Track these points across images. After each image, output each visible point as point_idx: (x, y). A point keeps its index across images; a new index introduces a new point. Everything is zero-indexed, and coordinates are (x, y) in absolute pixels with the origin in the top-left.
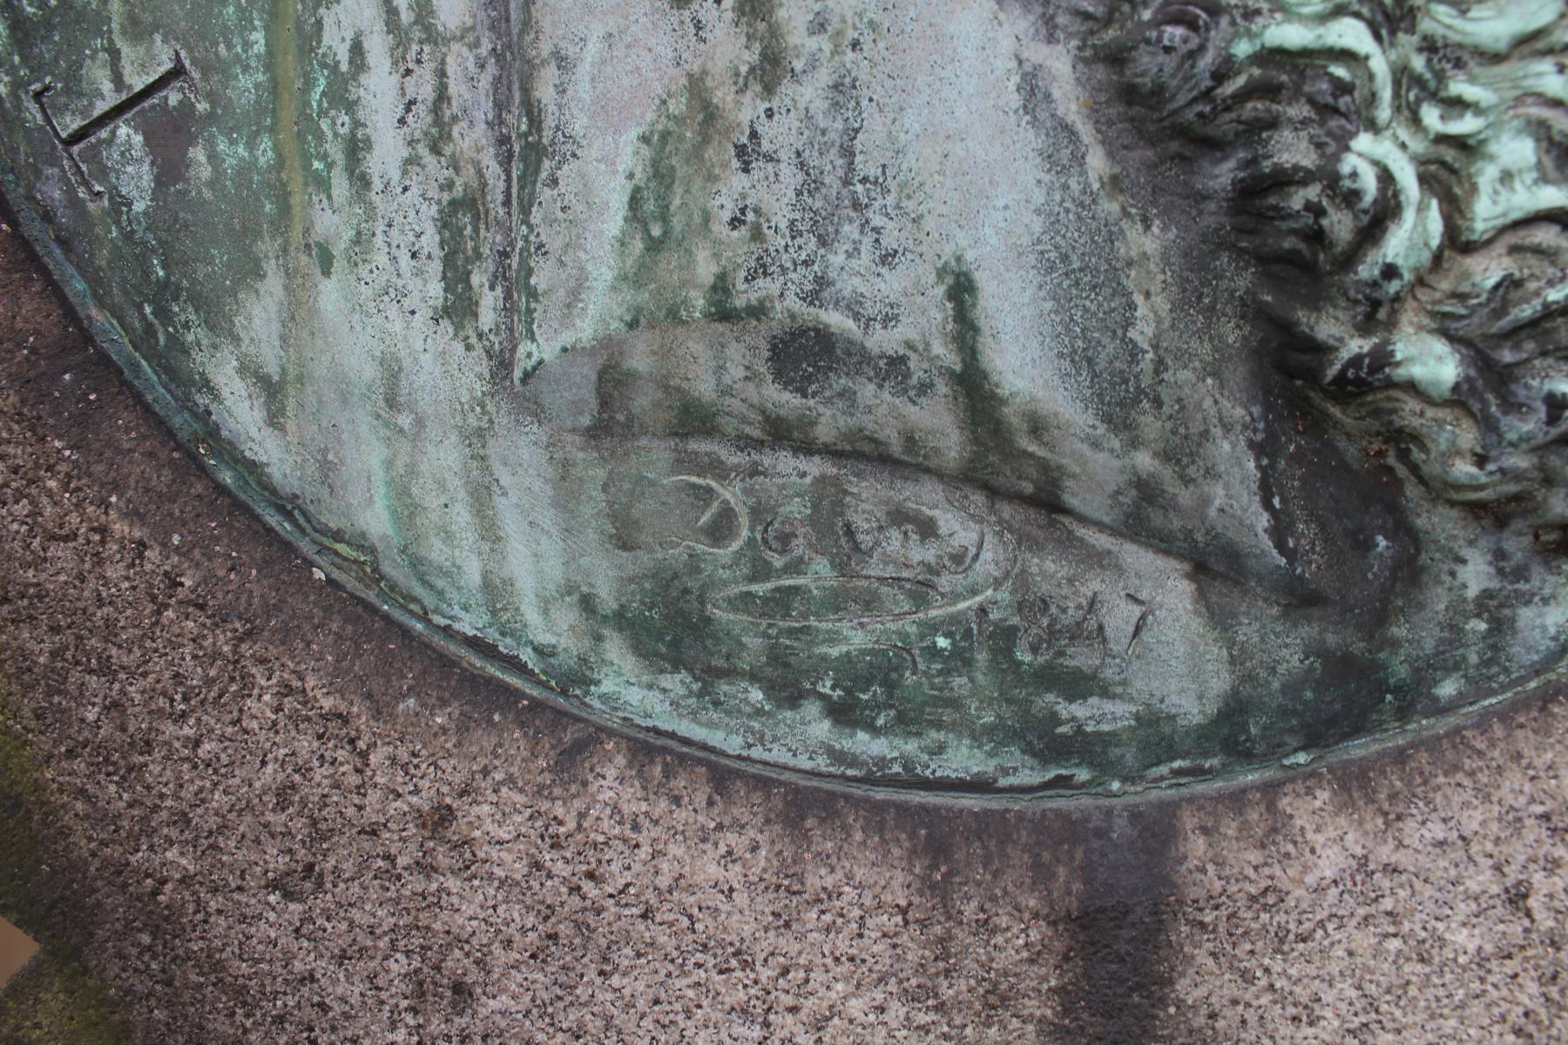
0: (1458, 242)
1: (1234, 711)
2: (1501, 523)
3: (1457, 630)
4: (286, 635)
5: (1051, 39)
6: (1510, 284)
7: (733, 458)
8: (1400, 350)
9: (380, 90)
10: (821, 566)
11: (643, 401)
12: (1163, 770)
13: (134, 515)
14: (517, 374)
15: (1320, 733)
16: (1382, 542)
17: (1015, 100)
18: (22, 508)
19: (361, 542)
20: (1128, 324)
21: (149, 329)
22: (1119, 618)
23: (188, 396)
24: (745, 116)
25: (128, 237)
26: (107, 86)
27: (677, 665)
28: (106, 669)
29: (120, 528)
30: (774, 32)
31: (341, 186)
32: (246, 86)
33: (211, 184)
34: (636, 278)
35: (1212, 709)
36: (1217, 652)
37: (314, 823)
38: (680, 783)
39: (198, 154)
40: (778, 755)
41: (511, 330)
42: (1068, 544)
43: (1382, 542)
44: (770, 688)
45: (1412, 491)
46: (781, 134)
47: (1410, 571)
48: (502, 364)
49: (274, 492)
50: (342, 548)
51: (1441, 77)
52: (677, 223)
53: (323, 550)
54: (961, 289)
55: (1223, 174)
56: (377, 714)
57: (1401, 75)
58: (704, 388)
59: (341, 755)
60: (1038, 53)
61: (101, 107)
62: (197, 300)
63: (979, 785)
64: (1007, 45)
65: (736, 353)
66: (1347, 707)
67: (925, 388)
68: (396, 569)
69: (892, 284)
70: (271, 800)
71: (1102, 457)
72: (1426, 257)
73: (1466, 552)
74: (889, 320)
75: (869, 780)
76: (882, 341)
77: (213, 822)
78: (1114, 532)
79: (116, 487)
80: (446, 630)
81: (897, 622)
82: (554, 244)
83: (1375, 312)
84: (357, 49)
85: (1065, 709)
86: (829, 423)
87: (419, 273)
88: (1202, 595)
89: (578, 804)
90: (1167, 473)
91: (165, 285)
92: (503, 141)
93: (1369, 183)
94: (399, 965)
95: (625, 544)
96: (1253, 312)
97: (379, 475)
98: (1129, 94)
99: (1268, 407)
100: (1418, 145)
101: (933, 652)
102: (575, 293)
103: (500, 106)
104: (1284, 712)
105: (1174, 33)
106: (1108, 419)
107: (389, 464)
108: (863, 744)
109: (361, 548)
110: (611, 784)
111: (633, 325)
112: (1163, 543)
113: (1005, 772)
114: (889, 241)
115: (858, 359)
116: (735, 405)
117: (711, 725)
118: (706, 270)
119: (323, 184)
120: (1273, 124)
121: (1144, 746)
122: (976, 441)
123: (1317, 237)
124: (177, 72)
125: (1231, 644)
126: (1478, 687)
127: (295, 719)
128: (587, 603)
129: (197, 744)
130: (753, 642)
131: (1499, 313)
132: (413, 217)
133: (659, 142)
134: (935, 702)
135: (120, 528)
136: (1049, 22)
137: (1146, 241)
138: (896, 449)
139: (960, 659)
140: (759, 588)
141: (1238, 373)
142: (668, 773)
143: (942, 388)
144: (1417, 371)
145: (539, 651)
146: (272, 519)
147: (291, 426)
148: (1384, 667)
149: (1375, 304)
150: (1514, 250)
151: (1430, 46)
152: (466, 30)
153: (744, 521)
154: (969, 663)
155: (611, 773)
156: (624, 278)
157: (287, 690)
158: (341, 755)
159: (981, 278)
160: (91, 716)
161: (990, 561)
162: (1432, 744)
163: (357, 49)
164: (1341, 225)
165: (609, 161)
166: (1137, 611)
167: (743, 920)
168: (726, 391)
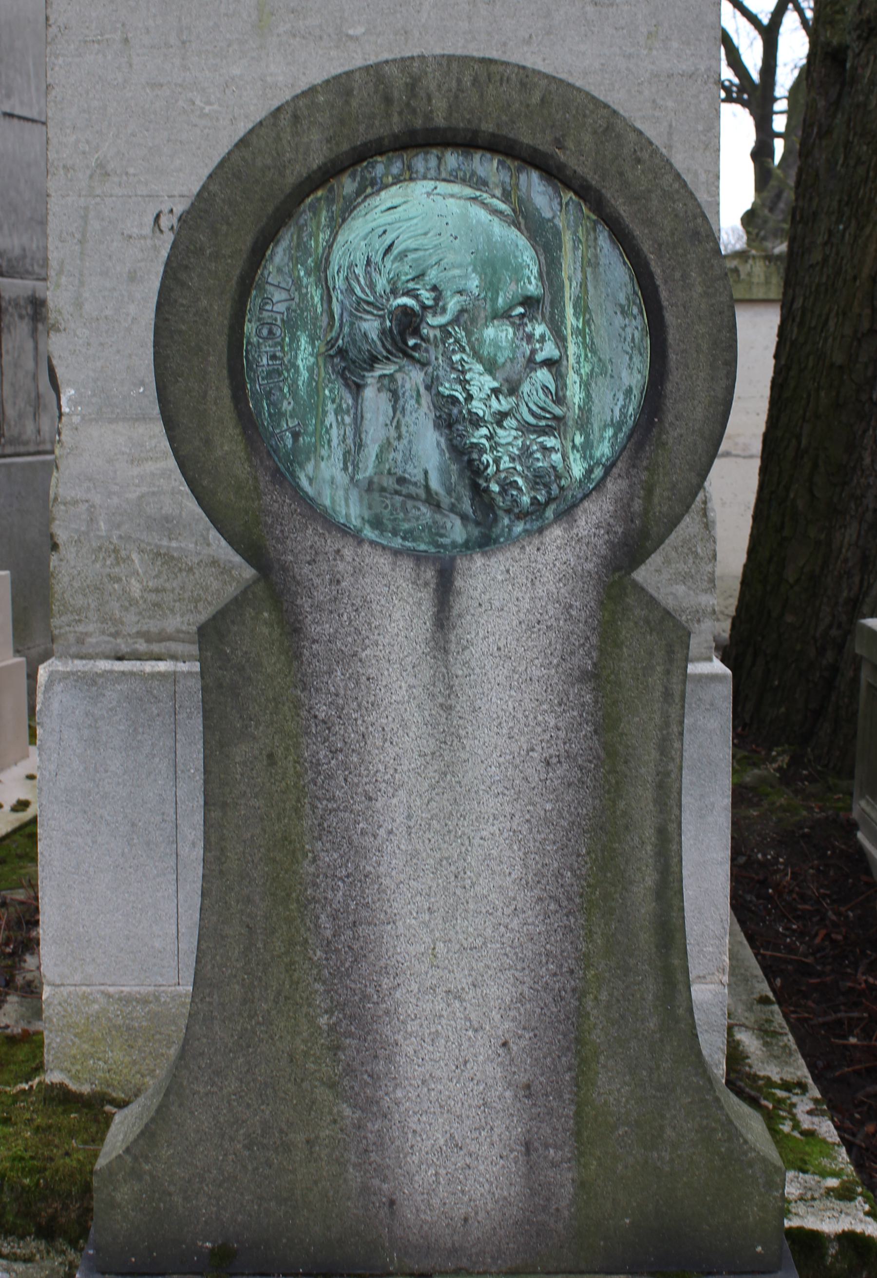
1: (467, 542)
9: (334, 432)
15: (481, 546)
19: (325, 506)
22: (449, 525)
28: (281, 524)
31: (326, 447)
32: (311, 429)
34: (376, 467)
39: (301, 439)
42: (441, 513)
46: (400, 447)
47: (496, 520)
48: (352, 479)
54: (426, 473)
55: (466, 458)
57: (491, 447)
58: (385, 485)
63: (426, 551)
66: (485, 542)
68: (330, 511)
69: (416, 471)
76: (413, 479)
81: (414, 524)
83: (487, 480)
86: (404, 491)
94: (328, 577)
96: (470, 478)
108: (407, 544)
110: (366, 547)
112: (456, 513)
115: (410, 482)
118: (387, 467)
126: (507, 540)
128: (363, 518)
132: (338, 453)
139: (423, 530)
141: (468, 488)
161: (428, 515)
164: (482, 467)
167: (387, 569)
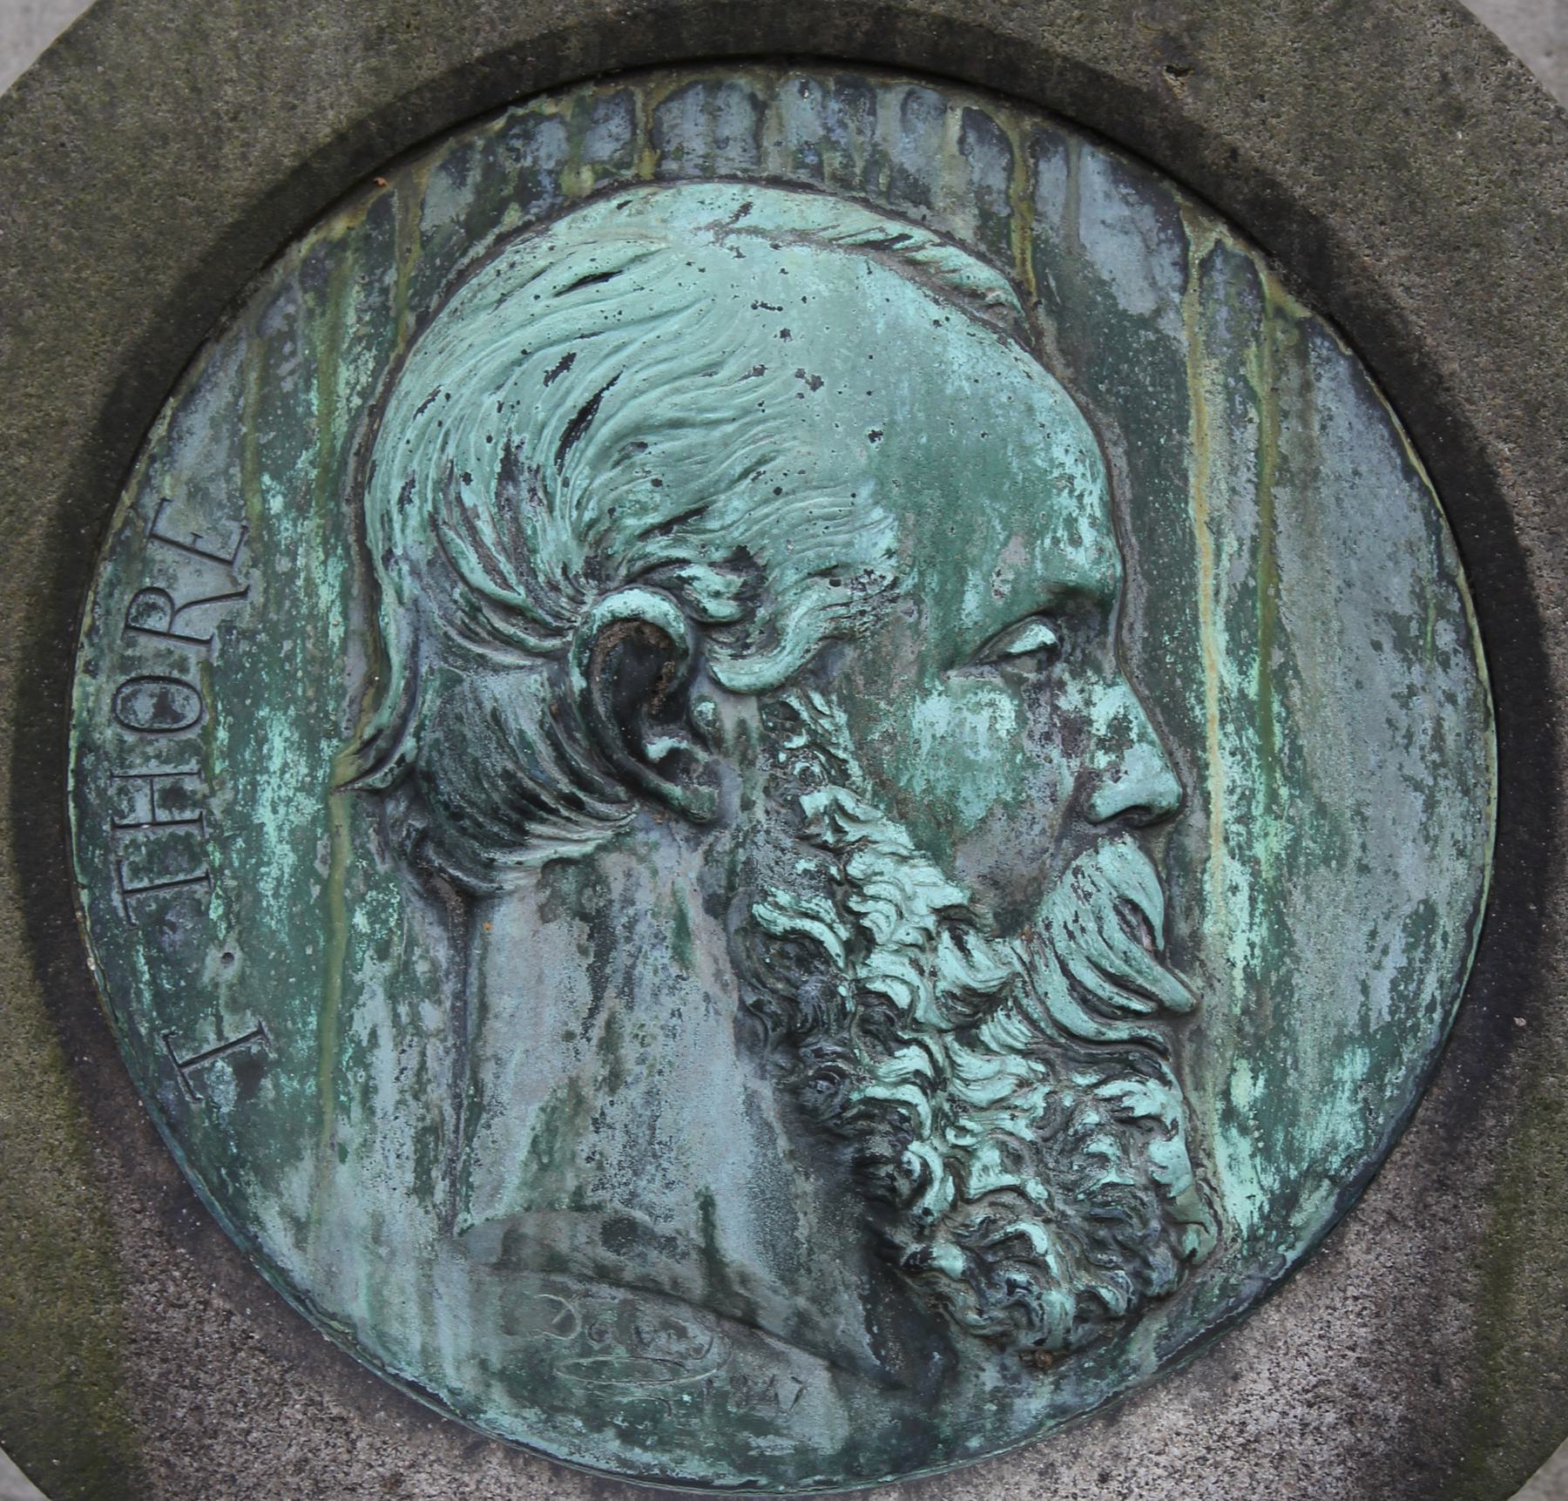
0: (962, 1198)
1: (851, 1448)
2: (1002, 1349)
3: (979, 1409)
4: (311, 1371)
5: (763, 1078)
6: (989, 1222)
7: (575, 1286)
8: (936, 1252)
9: (385, 1059)
10: (621, 1351)
11: (528, 1251)
12: (809, 1481)
13: (225, 1296)
14: (456, 1230)
16: (937, 1356)
17: (742, 1108)
18: (154, 1287)
19: (348, 1321)
20: (794, 1228)
21: (223, 1184)
22: (787, 1390)
23: (244, 1226)
24: (599, 1103)
25: (216, 1127)
26: (212, 1036)
27: (533, 1403)
28: (195, 1386)
29: (217, 1302)
30: (618, 1061)
31: (356, 1112)
33: (274, 1102)
34: (532, 1184)
35: (838, 1446)
36: (842, 1413)
37: (316, 1482)
38: (533, 1469)
39: (267, 1083)
40: (588, 1459)
41: (454, 1205)
42: (760, 1346)
43: (937, 1356)
44: (586, 1421)
45: (954, 1328)
46: (617, 1114)
47: (953, 1373)
48: (446, 1224)
49: (294, 1287)
50: (334, 1324)
51: (956, 1115)
52: (557, 1156)
53: (323, 1324)
54: (707, 1204)
55: (848, 1153)
56: (364, 1419)
57: (937, 1113)
58: (563, 1246)
59: (339, 1442)
60: (755, 1084)
61: (206, 1048)
62: (257, 1169)
63: (704, 1483)
64: (739, 1079)
65: (583, 1229)
67: (685, 1255)
68: (368, 1339)
69: (670, 1199)
70: (291, 1468)
71: (779, 1298)
72: (946, 1206)
73: (985, 1365)
74: (667, 1218)
75: (639, 1477)
76: (664, 1228)
77: (251, 1481)
78: (786, 1341)
79: (215, 1278)
80: (396, 1377)
82: (486, 1160)
83: (923, 1232)
84: (373, 1034)
85: (756, 1441)
86: (631, 1271)
87: (400, 1167)
88: (834, 1380)
89: (477, 1476)
90: (814, 1309)
91: (236, 1158)
92: (457, 1096)
93: (917, 1167)
95: (509, 1331)
97: (363, 1282)
98: (801, 1109)
99: (872, 1277)
100: (943, 1149)
101: (681, 1403)
102: (497, 1189)
103: (457, 1076)
104: (880, 1451)
105: (823, 1084)
106: (782, 1278)
107: (371, 1276)
108: (639, 1456)
109: (347, 1324)
110: (495, 1466)
111: (528, 1209)
112: (813, 1349)
113: (719, 1476)
114: (671, 1176)
115: (650, 1237)
116: (579, 1256)
117: (551, 1440)
118: (571, 1183)
119: (346, 1110)
120: (872, 1132)
121: (799, 1466)
122: (711, 1285)
123: (893, 1190)
124: (260, 1032)
125: (850, 1409)
126: (992, 1443)
127: (314, 1420)
128: (483, 1365)
129: (248, 1432)
130: (579, 1392)
131: (985, 1236)
132: (399, 1134)
133: (550, 1112)
134: (681, 1432)
135: (217, 1302)
136: (762, 1067)
137: (807, 1186)
138: (667, 1287)
139: (696, 1408)
140: (585, 1361)
141: (854, 1258)
142: (527, 1463)
143: (694, 1255)
144: (943, 1263)
145: (452, 1392)
146: (294, 1304)
147: (310, 1249)
148: (937, 1427)
149: (922, 1227)
150: (992, 1204)
151: (952, 1099)
152: (439, 1031)
153: (579, 1322)
154: (701, 1411)
155: (495, 1461)
156: (524, 1183)
157: (311, 1402)
158: (339, 1442)
159: (718, 1199)
160: (180, 1414)
161: (715, 1355)
162: (958, 1473)
163: (373, 1034)
164: (904, 1186)
165: (522, 1119)
166: (797, 1387)
168: (575, 1249)
